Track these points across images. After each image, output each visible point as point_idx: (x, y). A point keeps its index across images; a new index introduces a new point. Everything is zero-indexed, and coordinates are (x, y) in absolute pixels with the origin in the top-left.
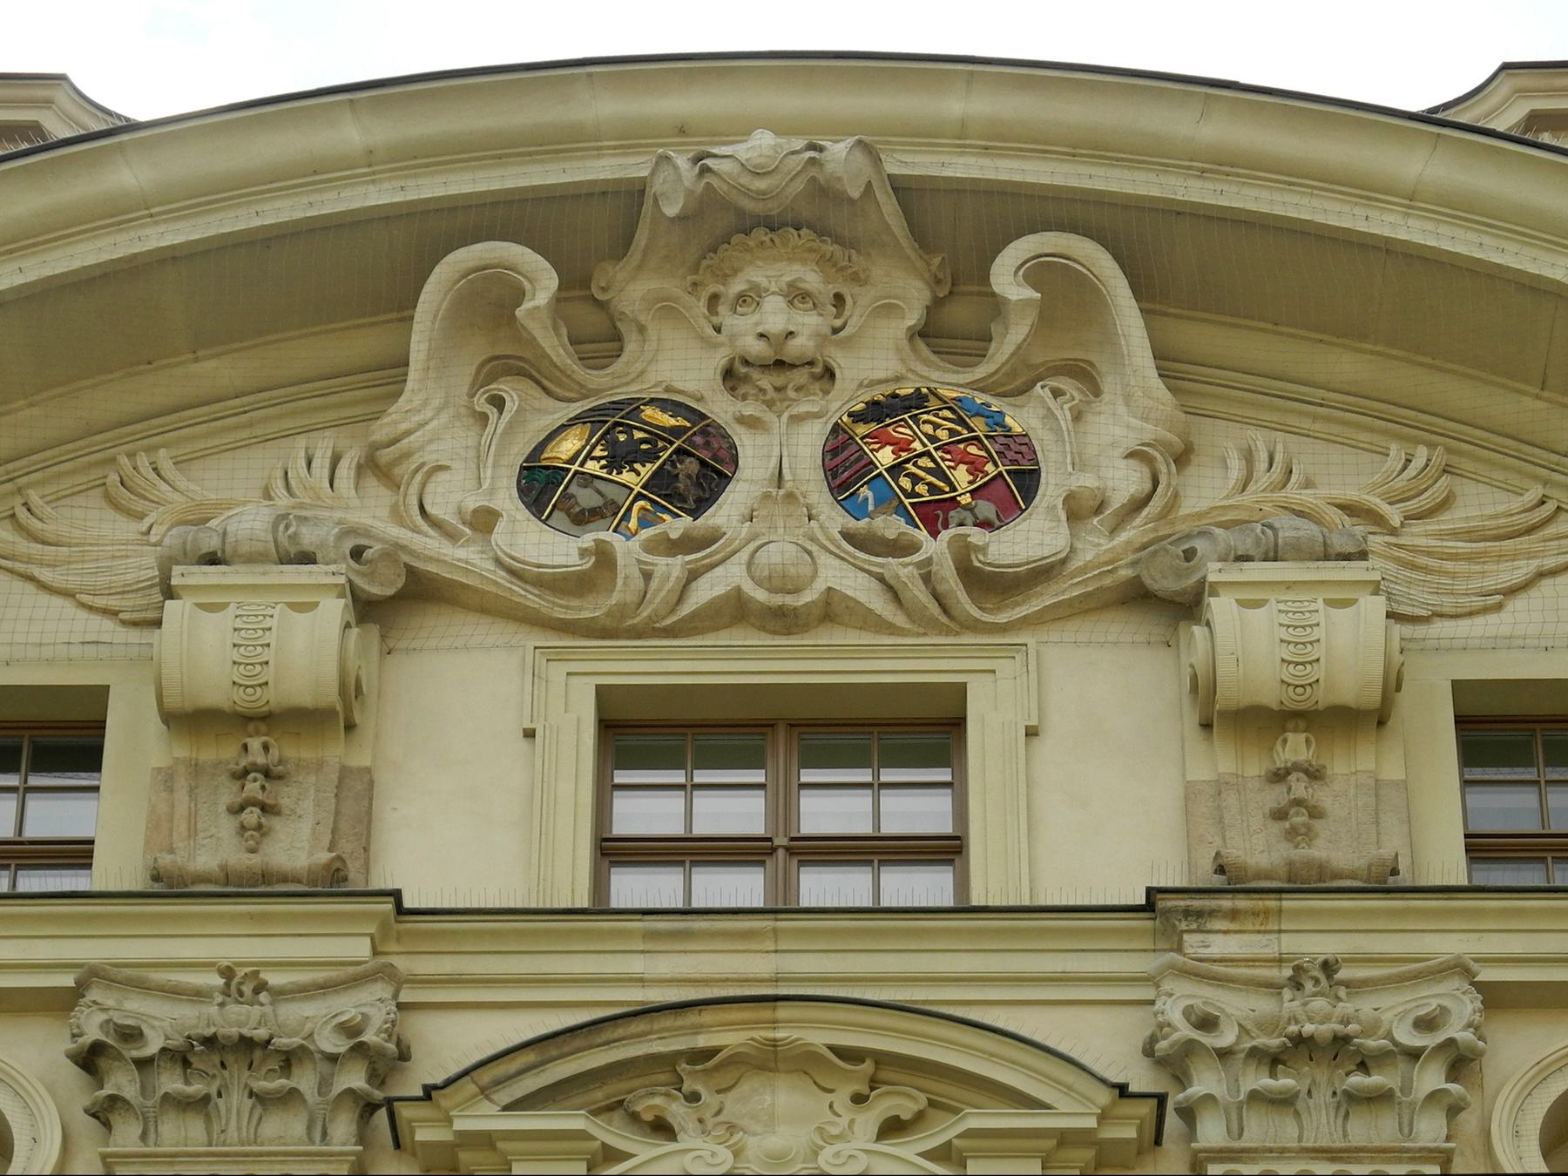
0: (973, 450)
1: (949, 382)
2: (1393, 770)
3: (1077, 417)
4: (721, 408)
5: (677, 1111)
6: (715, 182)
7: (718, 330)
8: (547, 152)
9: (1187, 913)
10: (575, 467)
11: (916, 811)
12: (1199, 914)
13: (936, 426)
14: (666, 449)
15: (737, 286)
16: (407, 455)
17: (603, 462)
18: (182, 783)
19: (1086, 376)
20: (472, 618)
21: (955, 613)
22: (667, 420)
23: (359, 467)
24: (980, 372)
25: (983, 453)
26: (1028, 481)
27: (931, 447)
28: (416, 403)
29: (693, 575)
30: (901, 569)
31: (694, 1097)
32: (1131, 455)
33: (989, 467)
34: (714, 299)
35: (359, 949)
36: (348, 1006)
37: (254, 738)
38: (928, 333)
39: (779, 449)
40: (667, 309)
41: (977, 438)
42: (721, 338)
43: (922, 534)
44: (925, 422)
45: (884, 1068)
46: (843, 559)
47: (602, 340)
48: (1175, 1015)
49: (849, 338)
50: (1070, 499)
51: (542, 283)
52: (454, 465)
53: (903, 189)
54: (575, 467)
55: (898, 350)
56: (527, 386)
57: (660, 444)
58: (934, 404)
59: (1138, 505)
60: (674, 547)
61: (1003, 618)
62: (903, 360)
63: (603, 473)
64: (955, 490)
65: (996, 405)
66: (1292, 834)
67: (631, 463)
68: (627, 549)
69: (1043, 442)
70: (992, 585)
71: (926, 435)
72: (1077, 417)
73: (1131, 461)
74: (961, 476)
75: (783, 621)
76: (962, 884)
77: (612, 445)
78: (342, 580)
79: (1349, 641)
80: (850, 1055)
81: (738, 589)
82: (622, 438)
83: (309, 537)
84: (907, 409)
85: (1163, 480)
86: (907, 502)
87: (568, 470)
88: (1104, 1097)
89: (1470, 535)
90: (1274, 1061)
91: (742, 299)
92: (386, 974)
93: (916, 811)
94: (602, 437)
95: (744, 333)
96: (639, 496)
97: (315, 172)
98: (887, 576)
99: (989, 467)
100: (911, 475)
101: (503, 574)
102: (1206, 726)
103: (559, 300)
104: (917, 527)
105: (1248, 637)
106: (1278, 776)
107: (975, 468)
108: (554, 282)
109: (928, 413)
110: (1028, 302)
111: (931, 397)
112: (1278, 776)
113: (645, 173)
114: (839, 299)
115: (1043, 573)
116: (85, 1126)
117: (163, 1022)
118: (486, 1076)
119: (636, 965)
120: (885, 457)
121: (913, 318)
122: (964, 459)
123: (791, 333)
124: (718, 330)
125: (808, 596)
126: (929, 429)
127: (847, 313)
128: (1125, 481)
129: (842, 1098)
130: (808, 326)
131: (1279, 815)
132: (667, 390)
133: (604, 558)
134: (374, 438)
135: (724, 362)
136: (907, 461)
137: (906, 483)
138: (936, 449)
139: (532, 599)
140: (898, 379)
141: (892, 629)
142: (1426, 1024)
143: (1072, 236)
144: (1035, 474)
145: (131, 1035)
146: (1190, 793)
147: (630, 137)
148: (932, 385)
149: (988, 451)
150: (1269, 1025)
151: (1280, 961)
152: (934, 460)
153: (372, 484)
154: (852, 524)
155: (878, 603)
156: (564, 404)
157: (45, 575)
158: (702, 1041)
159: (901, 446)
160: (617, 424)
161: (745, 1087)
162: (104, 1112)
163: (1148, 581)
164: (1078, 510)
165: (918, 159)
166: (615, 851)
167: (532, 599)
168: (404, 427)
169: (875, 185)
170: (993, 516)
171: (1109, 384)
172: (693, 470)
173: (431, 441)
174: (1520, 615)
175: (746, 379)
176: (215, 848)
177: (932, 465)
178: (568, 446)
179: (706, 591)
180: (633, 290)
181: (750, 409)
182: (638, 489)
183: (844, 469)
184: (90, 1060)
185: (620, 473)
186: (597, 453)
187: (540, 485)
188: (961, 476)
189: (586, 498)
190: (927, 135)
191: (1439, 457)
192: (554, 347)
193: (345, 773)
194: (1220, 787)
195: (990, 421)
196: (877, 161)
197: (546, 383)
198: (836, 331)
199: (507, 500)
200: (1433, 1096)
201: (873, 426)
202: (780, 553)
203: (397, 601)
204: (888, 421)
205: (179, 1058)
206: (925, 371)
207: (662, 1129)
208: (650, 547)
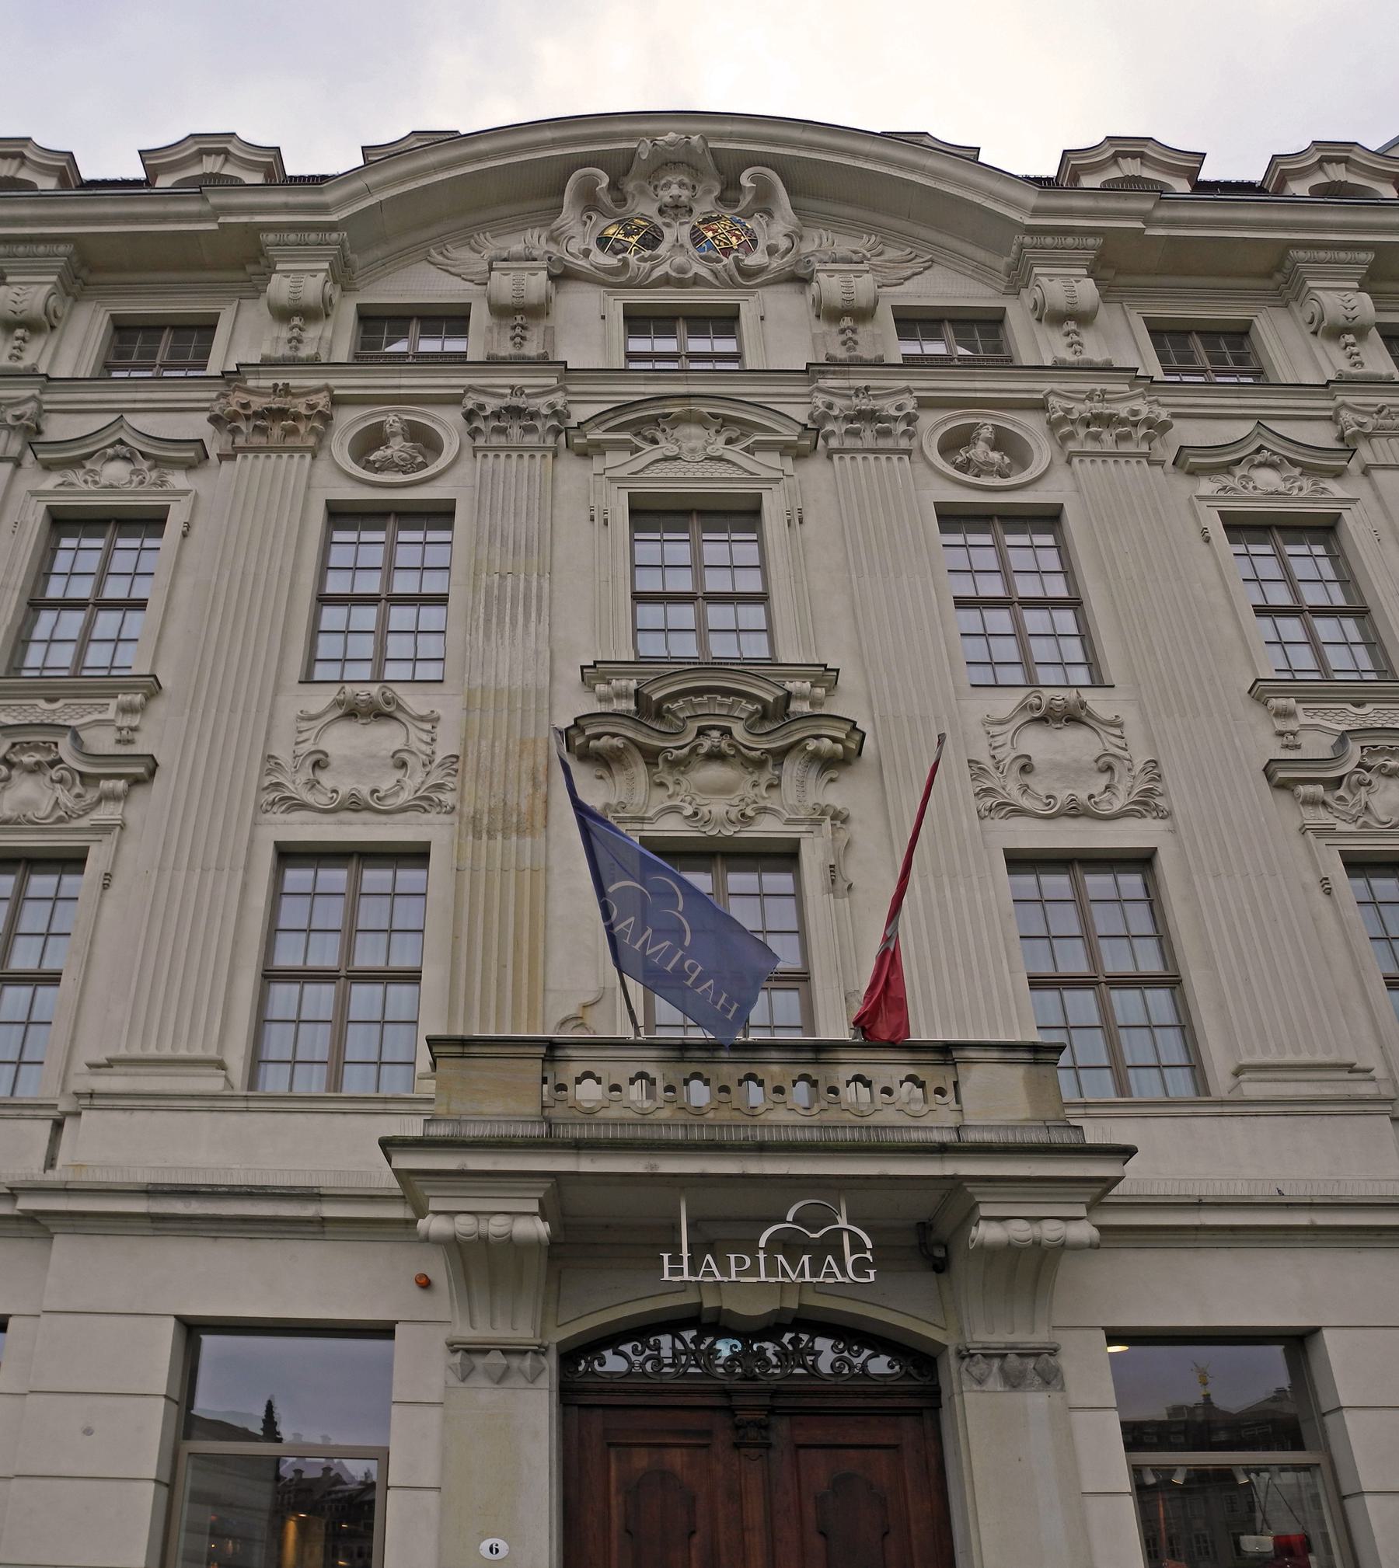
2: (877, 331)
4: (659, 221)
5: (659, 435)
9: (820, 372)
11: (727, 345)
12: (823, 372)
15: (663, 182)
18: (495, 330)
19: (769, 214)
26: (754, 242)
29: (652, 269)
30: (719, 266)
31: (664, 431)
34: (656, 187)
35: (554, 381)
36: (551, 398)
37: (520, 314)
38: (720, 199)
39: (677, 232)
40: (642, 192)
45: (727, 421)
47: (621, 201)
48: (820, 404)
50: (768, 247)
51: (605, 181)
53: (713, 151)
59: (788, 251)
66: (849, 349)
68: (632, 258)
69: (757, 230)
74: (734, 240)
75: (681, 283)
76: (743, 365)
79: (864, 287)
80: (715, 416)
83: (535, 253)
88: (799, 429)
89: (890, 261)
90: (850, 419)
92: (563, 389)
93: (727, 345)
95: (666, 196)
102: (818, 316)
105: (831, 286)
106: (843, 331)
107: (739, 238)
108: (607, 180)
112: (843, 331)
114: (694, 187)
115: (762, 270)
116: (467, 439)
117: (492, 404)
118: (598, 420)
119: (642, 389)
120: (710, 234)
121: (716, 193)
125: (690, 274)
128: (784, 243)
129: (712, 431)
130: (685, 194)
131: (844, 343)
133: (625, 261)
139: (602, 275)
141: (712, 286)
142: (899, 408)
145: (482, 407)
146: (814, 337)
147: (631, 136)
150: (849, 408)
151: (850, 388)
155: (711, 278)
157: (453, 270)
158: (667, 411)
159: (715, 231)
161: (681, 427)
162: (474, 433)
164: (771, 250)
166: (631, 357)
167: (602, 275)
171: (777, 215)
172: (651, 240)
174: (908, 286)
176: (506, 349)
178: (611, 231)
179: (657, 273)
181: (667, 220)
183: (697, 238)
184: (469, 416)
187: (603, 242)
188: (734, 240)
189: (618, 246)
190: (721, 137)
191: (879, 239)
192: (607, 199)
193: (546, 328)
194: (824, 335)
196: (706, 144)
199: (593, 247)
200: (904, 432)
202: (680, 260)
203: (563, 275)
205: (496, 415)
207: (654, 441)
208: (639, 260)
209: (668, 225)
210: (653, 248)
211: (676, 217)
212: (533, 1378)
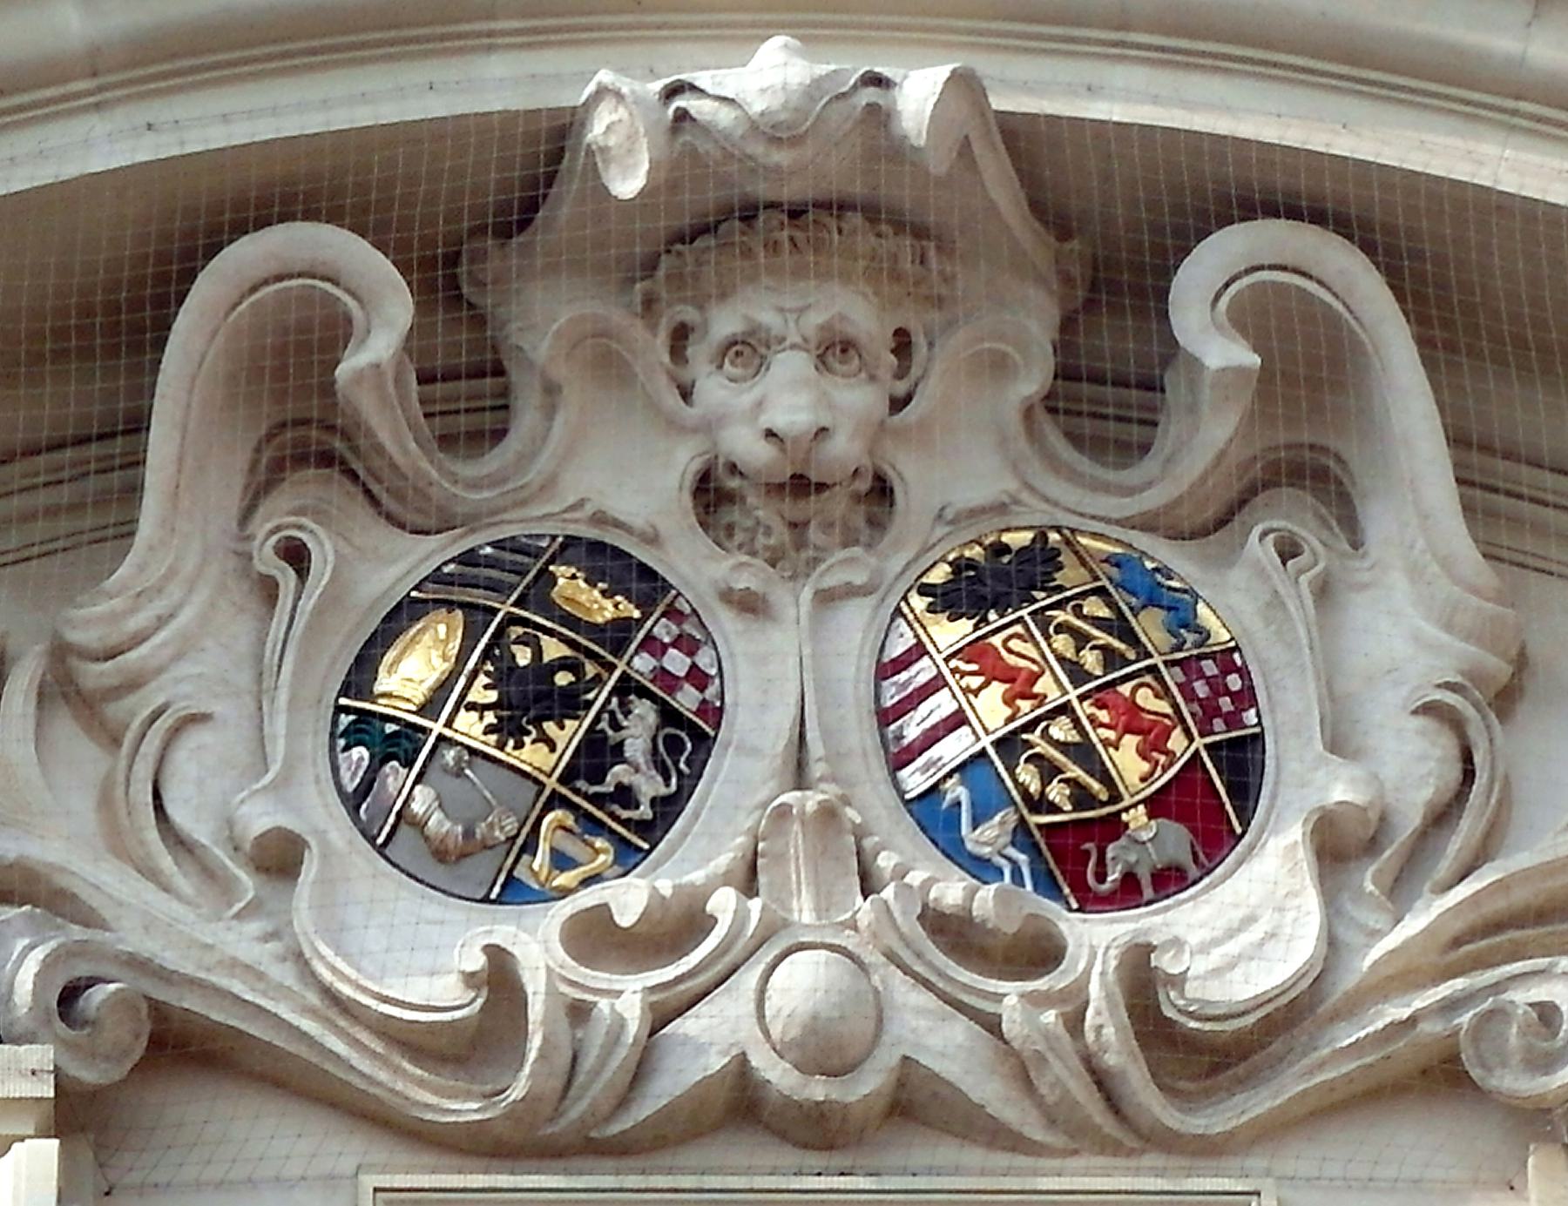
0: (1145, 698)
3: (1324, 591)
6: (704, 146)
7: (686, 394)
15: (725, 323)
16: (133, 684)
17: (490, 717)
21: (1129, 1111)
23: (43, 697)
24: (1151, 500)
25: (1164, 707)
28: (157, 572)
32: (1428, 709)
34: (681, 335)
40: (608, 364)
44: (1060, 628)
49: (924, 425)
52: (216, 708)
53: (1019, 136)
54: (438, 728)
55: (1003, 442)
57: (591, 669)
58: (1071, 576)
62: (1015, 468)
64: (1115, 798)
67: (537, 722)
70: (1199, 1056)
72: (1324, 591)
73: (1420, 722)
74: (1127, 761)
77: (505, 675)
81: (741, 1066)
82: (523, 657)
94: (486, 655)
100: (1036, 759)
103: (415, 342)
107: (1153, 743)
115: (1290, 1017)
121: (1033, 381)
122: (1131, 720)
123: (824, 429)
124: (686, 394)
127: (915, 371)
132: (600, 519)
133: (500, 977)
135: (697, 465)
136: (1030, 727)
137: (1028, 775)
140: (1001, 508)
141: (1015, 1142)
149: (1175, 706)
152: (1076, 723)
153: (65, 727)
159: (1020, 685)
168: (135, 623)
169: (977, 148)
173: (178, 657)
177: (1073, 737)
179: (714, 1034)
180: (546, 318)
185: (519, 745)
186: (479, 694)
188: (1127, 761)
198: (898, 404)
206: (1057, 488)
209: (750, 605)
210: (642, 834)
211: (793, 553)
212: (771, 1114)
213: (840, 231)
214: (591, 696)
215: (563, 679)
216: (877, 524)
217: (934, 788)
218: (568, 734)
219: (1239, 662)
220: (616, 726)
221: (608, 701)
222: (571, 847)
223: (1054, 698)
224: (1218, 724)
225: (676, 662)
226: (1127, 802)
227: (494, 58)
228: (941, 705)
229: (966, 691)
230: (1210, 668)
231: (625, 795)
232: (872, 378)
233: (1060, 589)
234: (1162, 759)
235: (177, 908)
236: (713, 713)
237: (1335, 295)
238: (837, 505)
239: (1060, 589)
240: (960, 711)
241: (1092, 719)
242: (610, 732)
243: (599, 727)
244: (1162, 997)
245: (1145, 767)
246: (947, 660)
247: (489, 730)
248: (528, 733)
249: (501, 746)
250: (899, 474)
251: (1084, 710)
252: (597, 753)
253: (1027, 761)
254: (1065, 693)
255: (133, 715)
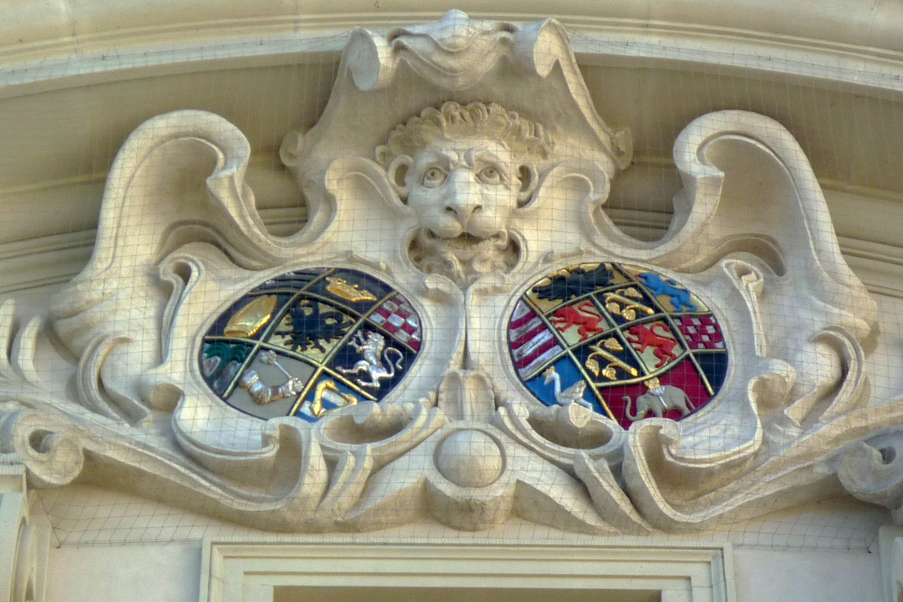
1: (634, 257)
7: (405, 200)
8: (246, 24)
10: (258, 343)
13: (623, 306)
14: (351, 324)
15: (426, 160)
17: (288, 338)
20: (149, 509)
22: (356, 295)
25: (669, 335)
27: (618, 329)
29: (380, 466)
33: (676, 350)
41: (664, 319)
42: (408, 209)
43: (612, 423)
44: (613, 301)
46: (532, 449)
47: (294, 209)
54: (258, 343)
56: (213, 253)
57: (346, 318)
58: (618, 280)
60: (361, 433)
61: (695, 518)
63: (288, 349)
65: (682, 281)
71: (613, 315)
78: (20, 470)
82: (308, 312)
84: (591, 286)
85: (853, 365)
86: (593, 385)
87: (252, 346)
91: (432, 172)
94: (287, 311)
96: (325, 375)
97: (21, 41)
98: (577, 470)
99: (676, 350)
101: (181, 458)
104: (609, 417)
107: (662, 351)
109: (613, 291)
110: (715, 181)
111: (616, 274)
113: (339, 45)
115: (735, 469)
126: (615, 308)
127: (533, 187)
134: (55, 307)
136: (594, 342)
137: (592, 365)
138: (623, 330)
140: (579, 253)
141: (581, 527)
143: (754, 115)
144: (722, 358)
148: (616, 261)
149: (673, 331)
154: (540, 409)
156: (247, 273)
159: (586, 326)
160: (302, 297)
163: (845, 482)
164: (772, 401)
165: (605, 37)
170: (682, 405)
175: (432, 252)
180: (334, 169)
182: (322, 367)
188: (648, 359)
195: (675, 300)
197: (231, 250)
201: (558, 304)
204: (574, 298)
213: (488, 111)
214: (346, 330)
215: (329, 321)
216: (511, 266)
217: (540, 374)
218: (332, 347)
219: (714, 321)
220: (360, 344)
221: (356, 332)
222: (333, 398)
223: (606, 329)
224: (701, 346)
225: (397, 321)
226: (649, 376)
227: (403, 528)
228: (543, 337)
229: (558, 329)
230: (696, 322)
231: (366, 376)
232: (507, 188)
233: (612, 284)
234: (668, 358)
235: (109, 421)
236: (418, 345)
237: (768, 147)
238: (489, 250)
239: (612, 284)
240: (555, 337)
241: (630, 340)
242: (356, 346)
243: (350, 343)
244: (665, 451)
245: (659, 361)
246: (547, 317)
247: (286, 344)
248: (309, 344)
249: (294, 349)
250: (523, 237)
251: (624, 336)
252: (348, 357)
253: (592, 358)
254: (613, 326)
255: (89, 341)
